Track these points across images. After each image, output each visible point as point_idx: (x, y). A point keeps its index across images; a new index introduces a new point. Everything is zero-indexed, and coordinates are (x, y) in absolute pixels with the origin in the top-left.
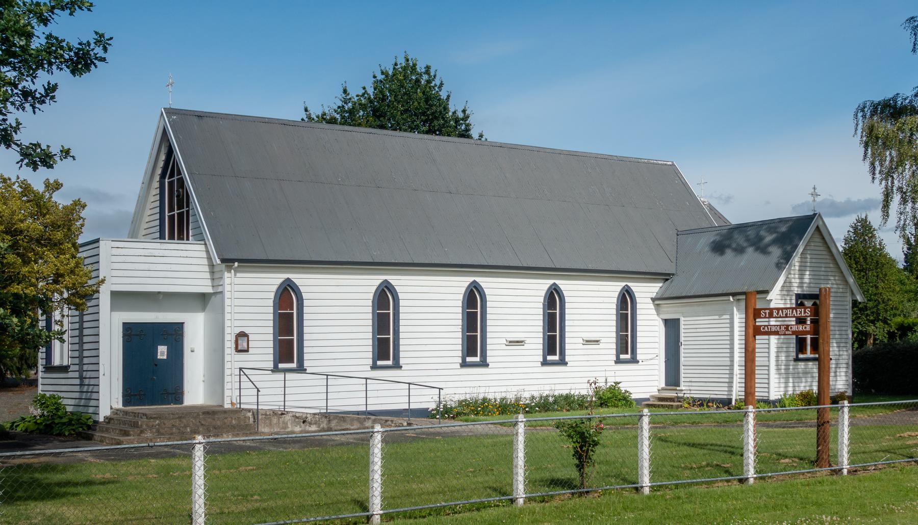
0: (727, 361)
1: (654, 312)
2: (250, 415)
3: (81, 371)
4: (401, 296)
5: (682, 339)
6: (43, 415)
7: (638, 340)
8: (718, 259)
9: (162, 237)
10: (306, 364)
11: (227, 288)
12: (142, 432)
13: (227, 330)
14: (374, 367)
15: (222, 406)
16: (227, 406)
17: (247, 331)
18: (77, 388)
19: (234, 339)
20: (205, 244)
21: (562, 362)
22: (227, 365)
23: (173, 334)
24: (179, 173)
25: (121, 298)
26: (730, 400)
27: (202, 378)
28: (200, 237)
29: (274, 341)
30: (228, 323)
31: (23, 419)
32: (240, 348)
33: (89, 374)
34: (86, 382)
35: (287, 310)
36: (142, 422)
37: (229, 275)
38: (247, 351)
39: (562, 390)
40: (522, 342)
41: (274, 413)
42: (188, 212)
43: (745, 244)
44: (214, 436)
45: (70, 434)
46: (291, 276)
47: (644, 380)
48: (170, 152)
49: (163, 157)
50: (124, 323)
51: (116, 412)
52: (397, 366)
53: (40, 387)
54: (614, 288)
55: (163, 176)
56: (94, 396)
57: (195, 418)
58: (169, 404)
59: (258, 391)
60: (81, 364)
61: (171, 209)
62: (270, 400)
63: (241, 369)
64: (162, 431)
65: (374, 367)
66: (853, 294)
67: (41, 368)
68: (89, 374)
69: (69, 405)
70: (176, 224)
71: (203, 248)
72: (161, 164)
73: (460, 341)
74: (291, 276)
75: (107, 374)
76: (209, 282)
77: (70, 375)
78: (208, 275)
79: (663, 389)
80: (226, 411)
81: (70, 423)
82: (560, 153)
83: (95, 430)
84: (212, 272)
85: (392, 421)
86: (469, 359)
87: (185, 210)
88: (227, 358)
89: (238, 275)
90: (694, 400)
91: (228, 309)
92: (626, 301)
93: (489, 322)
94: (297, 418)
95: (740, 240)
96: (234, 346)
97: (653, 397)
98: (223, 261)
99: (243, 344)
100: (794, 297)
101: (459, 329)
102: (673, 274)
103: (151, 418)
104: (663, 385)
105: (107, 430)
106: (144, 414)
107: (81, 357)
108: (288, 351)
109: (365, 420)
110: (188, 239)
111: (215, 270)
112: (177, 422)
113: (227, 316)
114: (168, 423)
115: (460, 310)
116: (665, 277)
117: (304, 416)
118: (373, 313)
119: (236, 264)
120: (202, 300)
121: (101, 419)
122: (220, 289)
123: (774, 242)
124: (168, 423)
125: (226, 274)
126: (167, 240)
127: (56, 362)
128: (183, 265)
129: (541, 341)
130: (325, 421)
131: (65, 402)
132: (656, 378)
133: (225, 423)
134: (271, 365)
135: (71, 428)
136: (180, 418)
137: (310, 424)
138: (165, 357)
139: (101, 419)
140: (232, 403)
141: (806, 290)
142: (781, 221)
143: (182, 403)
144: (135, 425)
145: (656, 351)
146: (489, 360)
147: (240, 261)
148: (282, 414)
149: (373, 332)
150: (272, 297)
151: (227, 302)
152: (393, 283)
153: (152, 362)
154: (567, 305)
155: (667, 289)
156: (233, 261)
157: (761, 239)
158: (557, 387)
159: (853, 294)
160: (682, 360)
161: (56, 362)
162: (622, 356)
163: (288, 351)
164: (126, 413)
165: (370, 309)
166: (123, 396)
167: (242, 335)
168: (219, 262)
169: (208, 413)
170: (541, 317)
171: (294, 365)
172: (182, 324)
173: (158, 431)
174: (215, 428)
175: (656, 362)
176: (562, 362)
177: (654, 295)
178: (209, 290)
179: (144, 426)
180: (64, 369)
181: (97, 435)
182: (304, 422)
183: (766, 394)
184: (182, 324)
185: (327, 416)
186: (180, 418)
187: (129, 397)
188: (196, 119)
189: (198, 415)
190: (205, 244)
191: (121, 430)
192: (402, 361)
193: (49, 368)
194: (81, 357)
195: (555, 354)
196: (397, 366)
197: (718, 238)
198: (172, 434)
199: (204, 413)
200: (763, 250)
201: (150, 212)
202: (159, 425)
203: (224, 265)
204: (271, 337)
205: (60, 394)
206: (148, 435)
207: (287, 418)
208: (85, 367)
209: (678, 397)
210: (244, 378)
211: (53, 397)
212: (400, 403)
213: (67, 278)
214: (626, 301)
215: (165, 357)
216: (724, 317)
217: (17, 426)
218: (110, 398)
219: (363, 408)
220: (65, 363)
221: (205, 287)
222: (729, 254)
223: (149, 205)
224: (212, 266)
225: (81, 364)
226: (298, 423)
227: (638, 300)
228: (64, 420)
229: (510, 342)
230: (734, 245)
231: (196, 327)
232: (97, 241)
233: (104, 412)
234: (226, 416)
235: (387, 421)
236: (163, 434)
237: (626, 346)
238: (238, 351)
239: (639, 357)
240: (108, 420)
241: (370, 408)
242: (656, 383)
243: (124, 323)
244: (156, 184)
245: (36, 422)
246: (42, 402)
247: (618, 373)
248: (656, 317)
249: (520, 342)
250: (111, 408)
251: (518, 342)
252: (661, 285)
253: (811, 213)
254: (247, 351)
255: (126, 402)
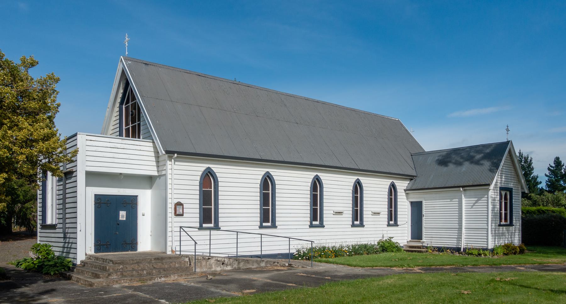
0: (457, 226)
1: (405, 197)
2: (187, 259)
3: (64, 228)
4: (276, 182)
5: (424, 213)
6: (39, 258)
7: (399, 213)
8: (444, 169)
9: (121, 135)
10: (220, 224)
11: (169, 172)
12: (109, 275)
13: (169, 201)
14: (261, 227)
15: (165, 253)
16: (169, 252)
17: (182, 201)
18: (62, 240)
19: (173, 207)
20: (153, 142)
21: (322, 225)
22: (169, 225)
23: (130, 204)
24: (134, 98)
25: (93, 177)
26: (460, 248)
27: (150, 233)
28: (149, 137)
29: (200, 208)
30: (169, 196)
31: (26, 260)
32: (178, 213)
33: (70, 230)
34: (68, 235)
35: (208, 187)
36: (109, 266)
37: (170, 163)
38: (182, 215)
39: (364, 242)
40: (341, 213)
41: (204, 258)
42: (139, 125)
43: (462, 160)
44: (164, 277)
45: (55, 274)
46: (211, 166)
47: (402, 235)
48: (127, 84)
49: (121, 91)
50: (95, 195)
51: (89, 257)
52: (274, 226)
53: (39, 238)
54: (387, 183)
55: (121, 103)
56: (73, 246)
57: (149, 263)
58: (127, 251)
59: (196, 243)
60: (64, 223)
61: (127, 124)
62: (203, 249)
63: (181, 227)
64: (125, 274)
65: (261, 227)
66: (522, 188)
67: (39, 226)
68: (70, 230)
69: (57, 251)
70: (132, 123)
71: (151, 144)
72: (120, 95)
73: (309, 212)
74: (211, 166)
75: (83, 230)
76: (155, 168)
77: (57, 231)
78: (154, 164)
79: (410, 241)
80: (170, 258)
81: (55, 265)
82: (347, 109)
83: (73, 271)
84: (158, 162)
85: (278, 263)
86: (264, 224)
87: (137, 123)
88: (169, 220)
89: (176, 163)
90: (434, 248)
91: (169, 186)
92: (393, 189)
93: (324, 201)
94: (219, 261)
95: (455, 157)
96: (173, 212)
97: (405, 245)
98: (167, 152)
99: (180, 211)
100: (498, 189)
101: (309, 204)
102: (416, 176)
103: (116, 263)
104: (410, 239)
105: (82, 273)
106: (110, 260)
107: (64, 219)
108: (208, 215)
109: (260, 261)
110: (139, 137)
111: (160, 159)
112: (136, 267)
113: (169, 191)
114: (129, 268)
115: (309, 192)
116: (411, 178)
117: (223, 260)
118: (260, 192)
119: (176, 155)
120: (149, 181)
121: (78, 263)
122: (164, 173)
123: (484, 158)
124: (129, 268)
125: (169, 162)
126: (124, 137)
127: (49, 222)
128: (136, 156)
129: (351, 212)
130: (236, 263)
131: (54, 249)
132: (406, 235)
133: (171, 266)
134: (198, 225)
135: (56, 269)
136: (138, 263)
137: (227, 265)
138: (125, 219)
139: (78, 263)
140: (172, 251)
141: (503, 185)
142: (489, 146)
143: (136, 250)
144: (104, 269)
145: (406, 219)
146: (325, 223)
147: (179, 153)
148: (209, 259)
149: (260, 205)
150: (199, 179)
151: (169, 181)
152: (272, 174)
153: (115, 222)
154: (364, 192)
155: (413, 184)
156: (174, 153)
157: (473, 157)
158: (362, 240)
159: (522, 188)
160: (424, 225)
161: (49, 222)
162: (314, 223)
163: (208, 215)
164: (97, 258)
165: (258, 190)
166: (95, 246)
167: (179, 204)
168: (164, 152)
169: (158, 259)
170: (351, 198)
171: (212, 225)
172: (135, 198)
173: (122, 274)
174: (164, 270)
175: (406, 226)
176: (322, 225)
177: (405, 188)
178: (155, 173)
179: (111, 270)
180: (53, 227)
181: (75, 276)
182: (223, 264)
183: (486, 245)
184: (135, 198)
185: (237, 258)
186: (138, 263)
187: (99, 247)
188: (144, 65)
189: (151, 260)
190: (153, 142)
191: (93, 273)
192: (277, 223)
193: (45, 226)
194: (64, 219)
195: (269, 222)
196: (274, 226)
197: (440, 158)
198: (132, 276)
199: (155, 259)
200: (477, 163)
201: (112, 128)
202: (122, 269)
203: (167, 156)
204: (198, 206)
205: (50, 244)
206: (114, 277)
207: (212, 261)
208: (67, 226)
209: (423, 246)
210: (183, 233)
211: (46, 245)
212: (284, 250)
213: (41, 144)
214: (393, 189)
215: (125, 219)
216: (483, 199)
217: (21, 265)
218: (85, 246)
219: (259, 253)
220: (54, 223)
221: (153, 172)
222: (451, 166)
223: (113, 123)
224: (157, 156)
225: (64, 223)
226: (219, 265)
227: (398, 190)
228: (51, 263)
229: (336, 213)
230: (454, 161)
231: (146, 200)
232: (75, 135)
233: (80, 257)
234: (171, 260)
235: (274, 262)
236: (125, 276)
237: (393, 218)
238: (176, 215)
239: (399, 223)
240: (84, 263)
241: (263, 253)
242: (406, 238)
243: (95, 195)
244: (117, 109)
245: (33, 263)
246: (36, 248)
247: (389, 232)
248: (406, 200)
249: (340, 213)
250: (86, 255)
251: (339, 213)
252: (408, 182)
253: (506, 141)
254: (182, 215)
255: (97, 250)
